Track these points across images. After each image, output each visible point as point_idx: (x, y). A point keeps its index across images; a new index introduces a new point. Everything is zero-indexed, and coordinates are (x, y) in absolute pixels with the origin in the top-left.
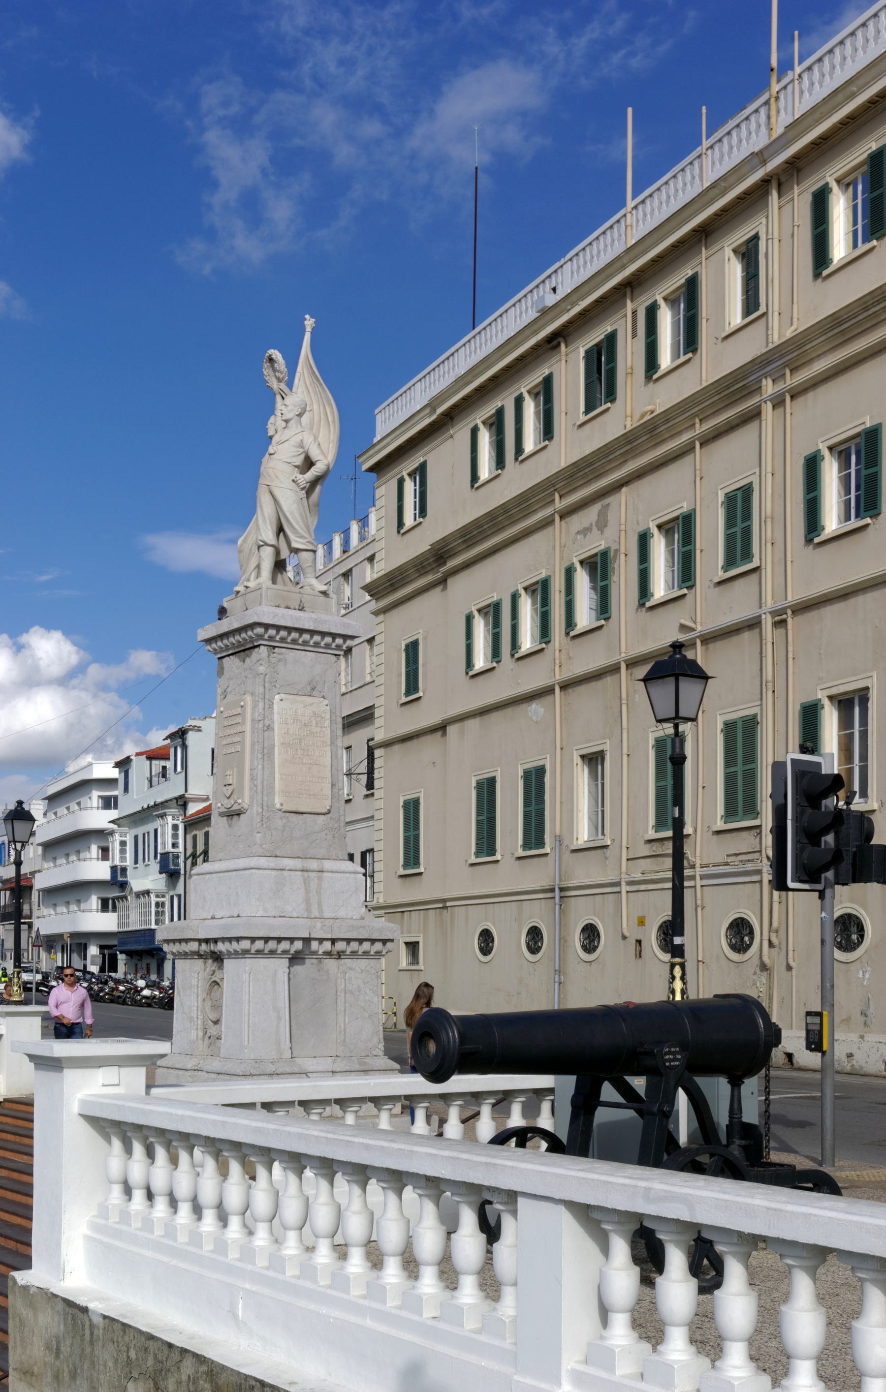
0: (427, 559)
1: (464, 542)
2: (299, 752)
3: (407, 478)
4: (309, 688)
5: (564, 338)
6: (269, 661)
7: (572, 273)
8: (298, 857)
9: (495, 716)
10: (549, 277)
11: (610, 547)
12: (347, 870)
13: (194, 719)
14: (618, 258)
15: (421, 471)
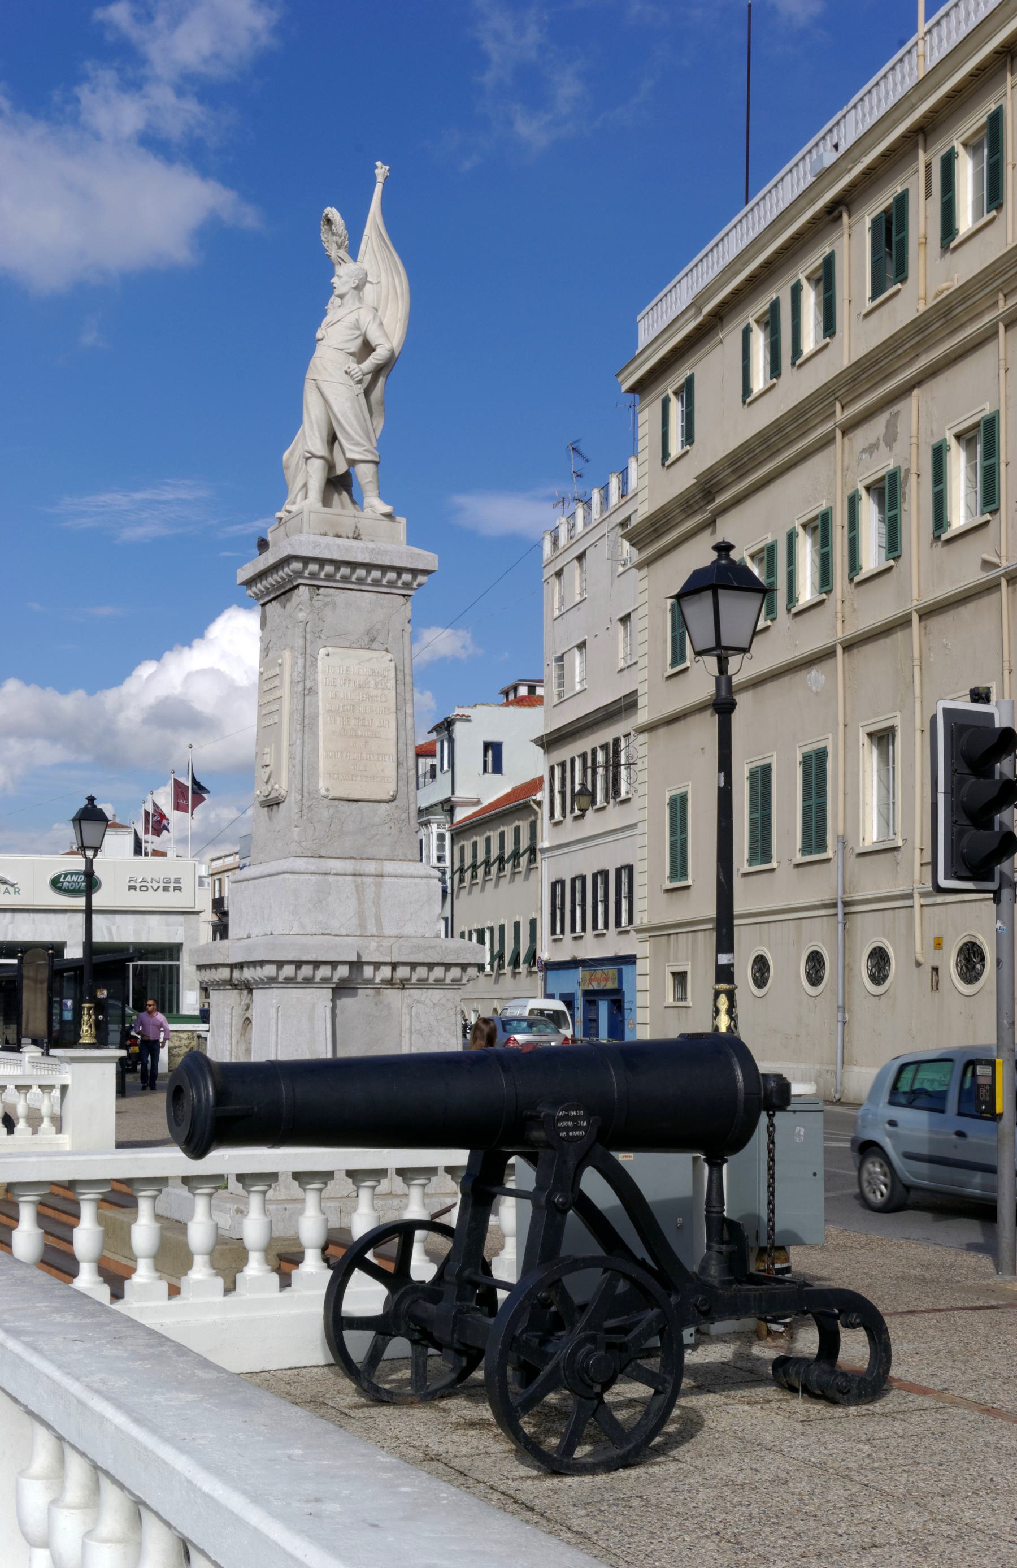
0: (694, 496)
1: (733, 472)
2: (352, 722)
3: (672, 397)
4: (367, 639)
5: (847, 206)
6: (312, 606)
7: (857, 123)
8: (351, 858)
9: (770, 687)
10: (830, 131)
11: (899, 467)
12: (416, 873)
13: (463, 707)
14: (905, 97)
15: (687, 391)
